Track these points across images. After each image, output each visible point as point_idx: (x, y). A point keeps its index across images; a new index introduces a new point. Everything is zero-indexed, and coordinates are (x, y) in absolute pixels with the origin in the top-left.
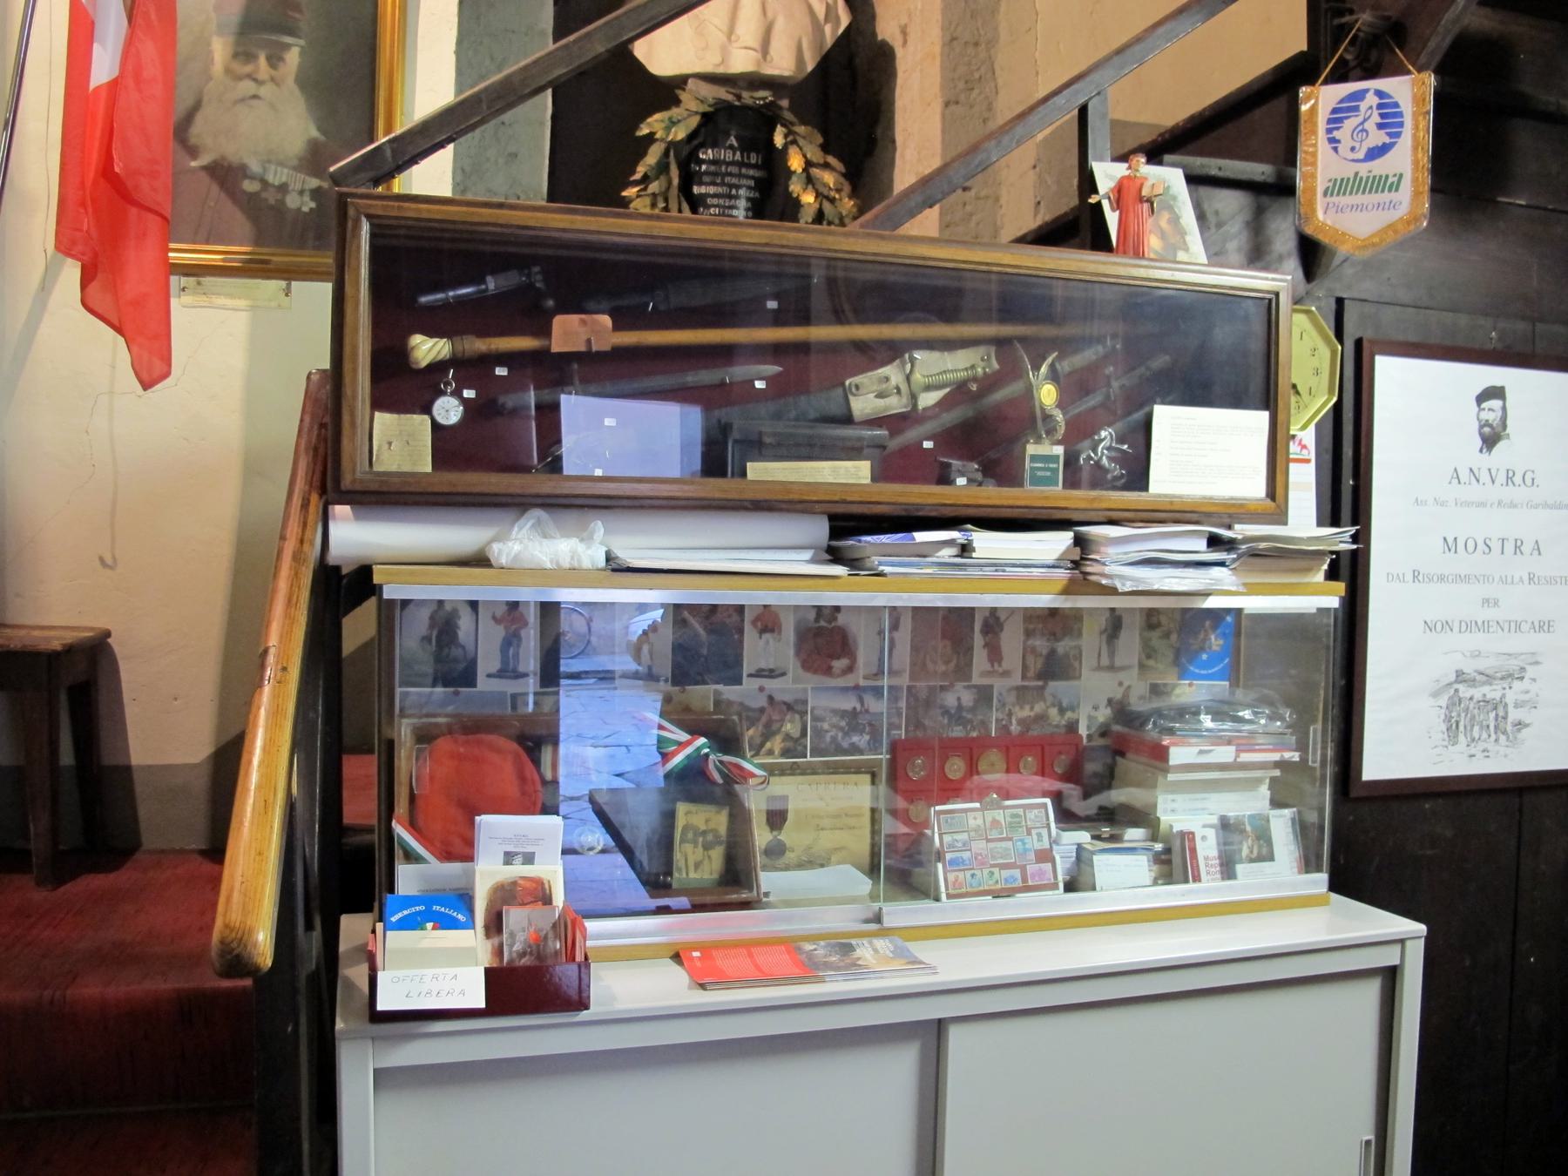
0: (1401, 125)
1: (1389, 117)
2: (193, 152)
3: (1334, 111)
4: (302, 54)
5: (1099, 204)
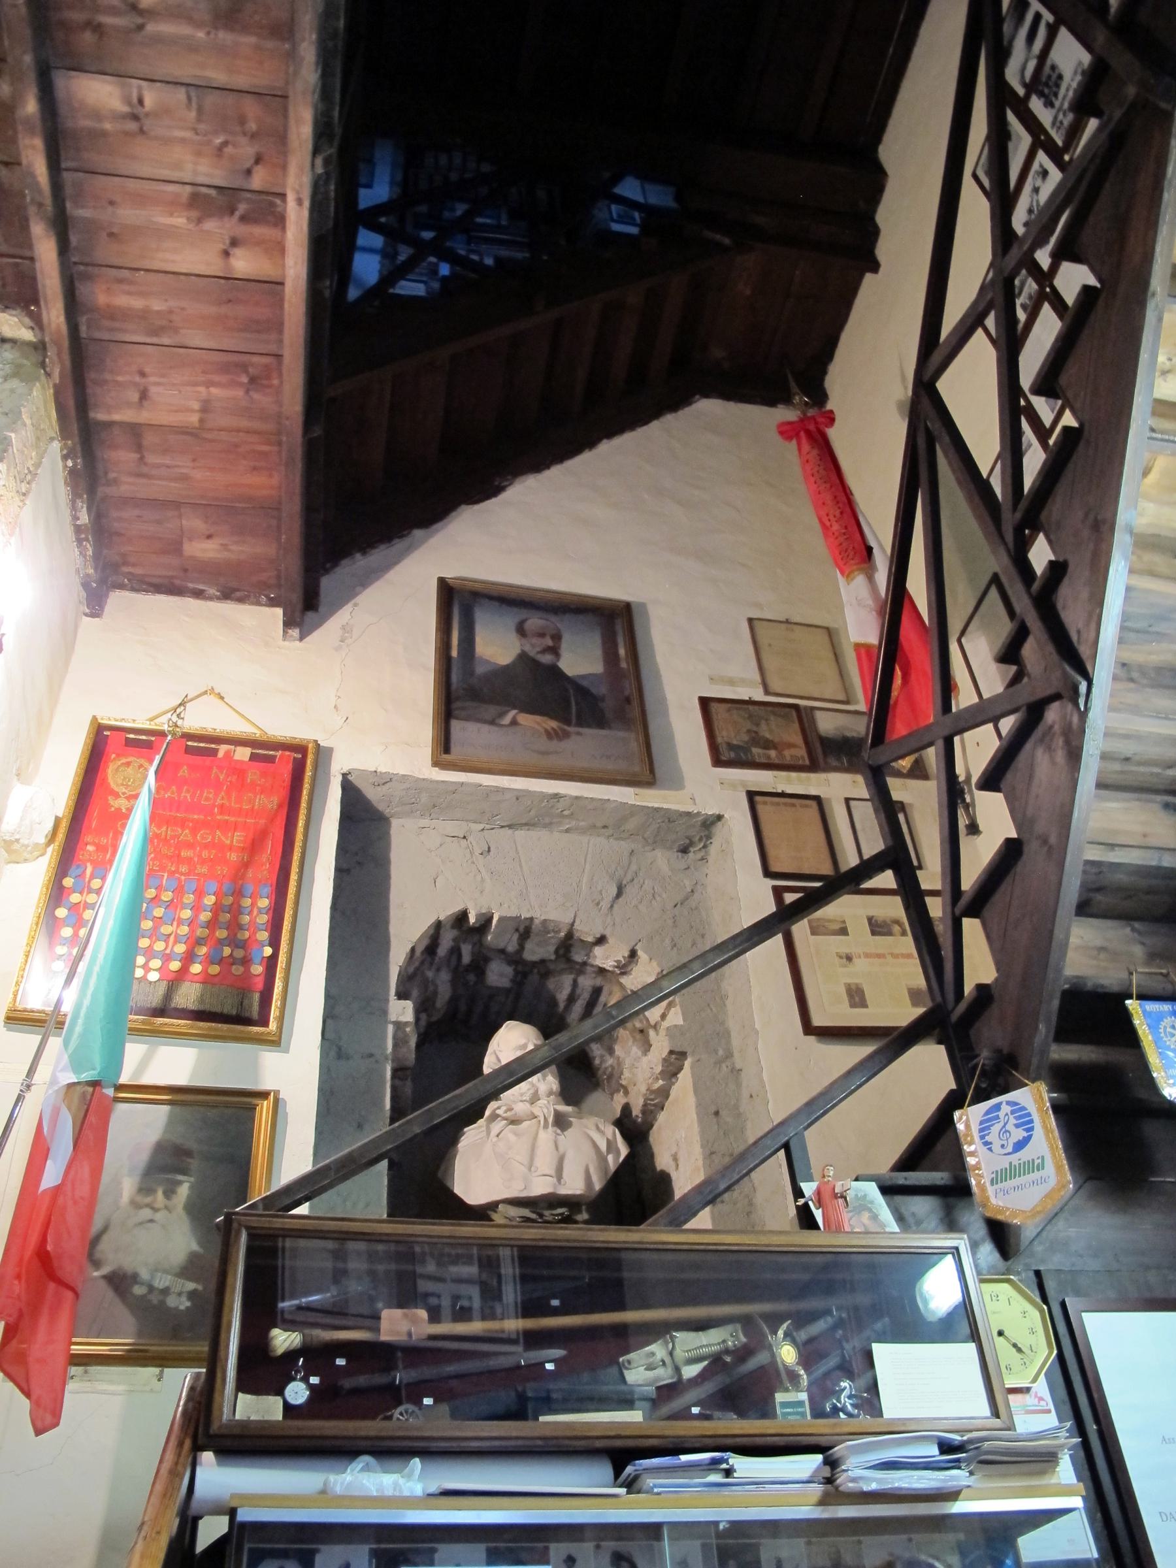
0: (1031, 1121)
1: (1026, 1123)
2: (97, 1264)
3: (981, 1123)
4: (191, 1188)
5: (806, 1205)
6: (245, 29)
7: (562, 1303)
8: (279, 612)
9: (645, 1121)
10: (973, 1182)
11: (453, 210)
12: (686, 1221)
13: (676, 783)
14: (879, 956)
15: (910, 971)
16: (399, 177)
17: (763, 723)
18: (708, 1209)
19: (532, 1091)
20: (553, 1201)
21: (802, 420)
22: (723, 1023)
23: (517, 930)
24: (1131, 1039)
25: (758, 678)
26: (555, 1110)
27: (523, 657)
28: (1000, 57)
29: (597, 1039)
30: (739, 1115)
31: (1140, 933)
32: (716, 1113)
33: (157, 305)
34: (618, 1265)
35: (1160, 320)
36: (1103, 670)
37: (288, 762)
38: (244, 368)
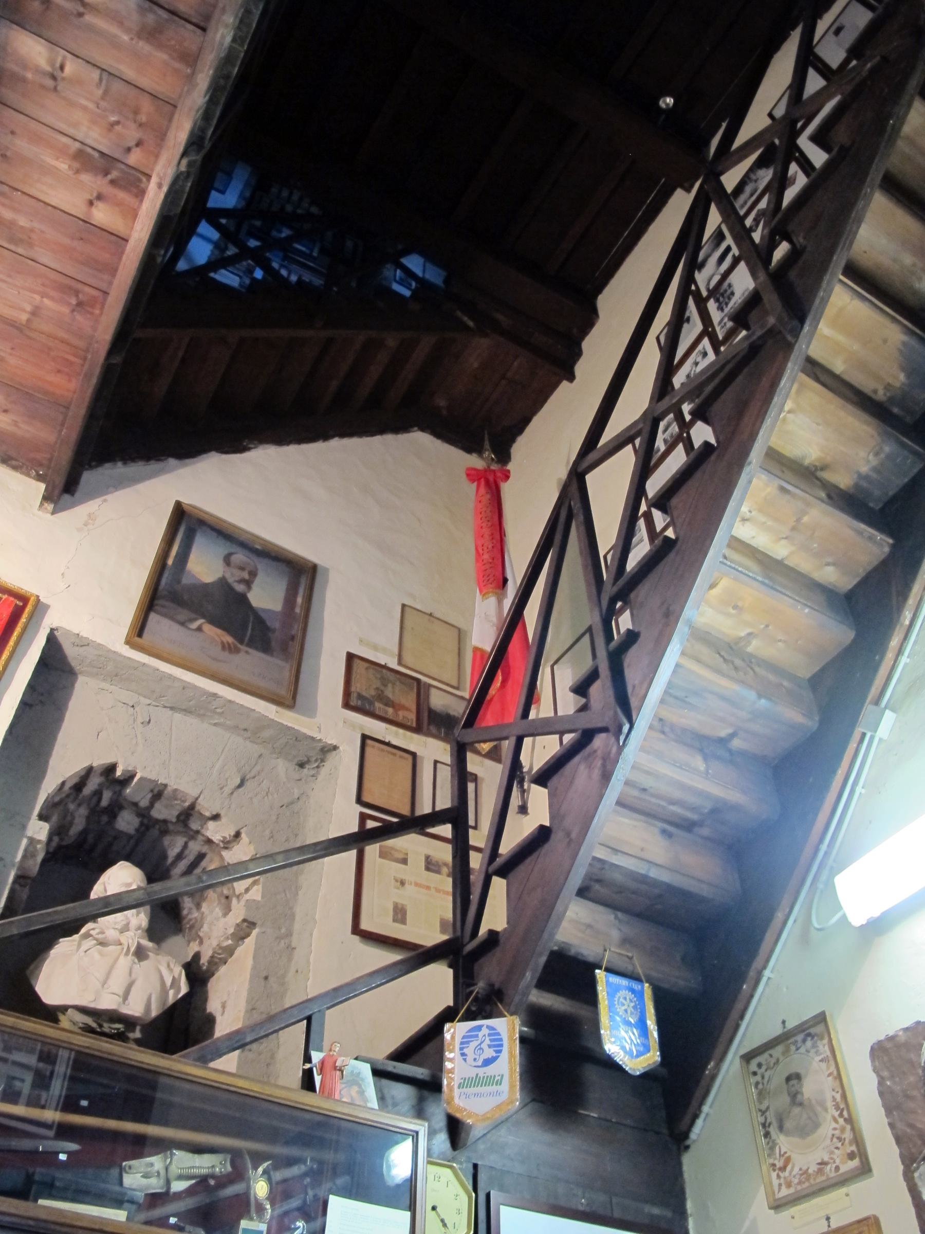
0: (501, 1045)
1: (497, 1046)
3: (464, 1037)
6: (160, 46)
7: (89, 1104)
8: (42, 486)
9: (208, 971)
10: (445, 1082)
11: (280, 232)
12: (212, 1060)
13: (310, 711)
14: (428, 888)
15: (444, 906)
16: (248, 194)
17: (390, 685)
18: (237, 1052)
19: (124, 923)
20: (114, 1016)
21: (485, 471)
22: (291, 908)
23: (152, 791)
24: (592, 1000)
25: (396, 651)
26: (138, 943)
27: (223, 582)
28: (694, 265)
29: (191, 894)
30: (283, 984)
31: (620, 921)
32: (264, 977)
33: (23, 222)
34: (153, 1086)
35: (750, 482)
36: (644, 719)
37: (9, 606)
38: (77, 293)
